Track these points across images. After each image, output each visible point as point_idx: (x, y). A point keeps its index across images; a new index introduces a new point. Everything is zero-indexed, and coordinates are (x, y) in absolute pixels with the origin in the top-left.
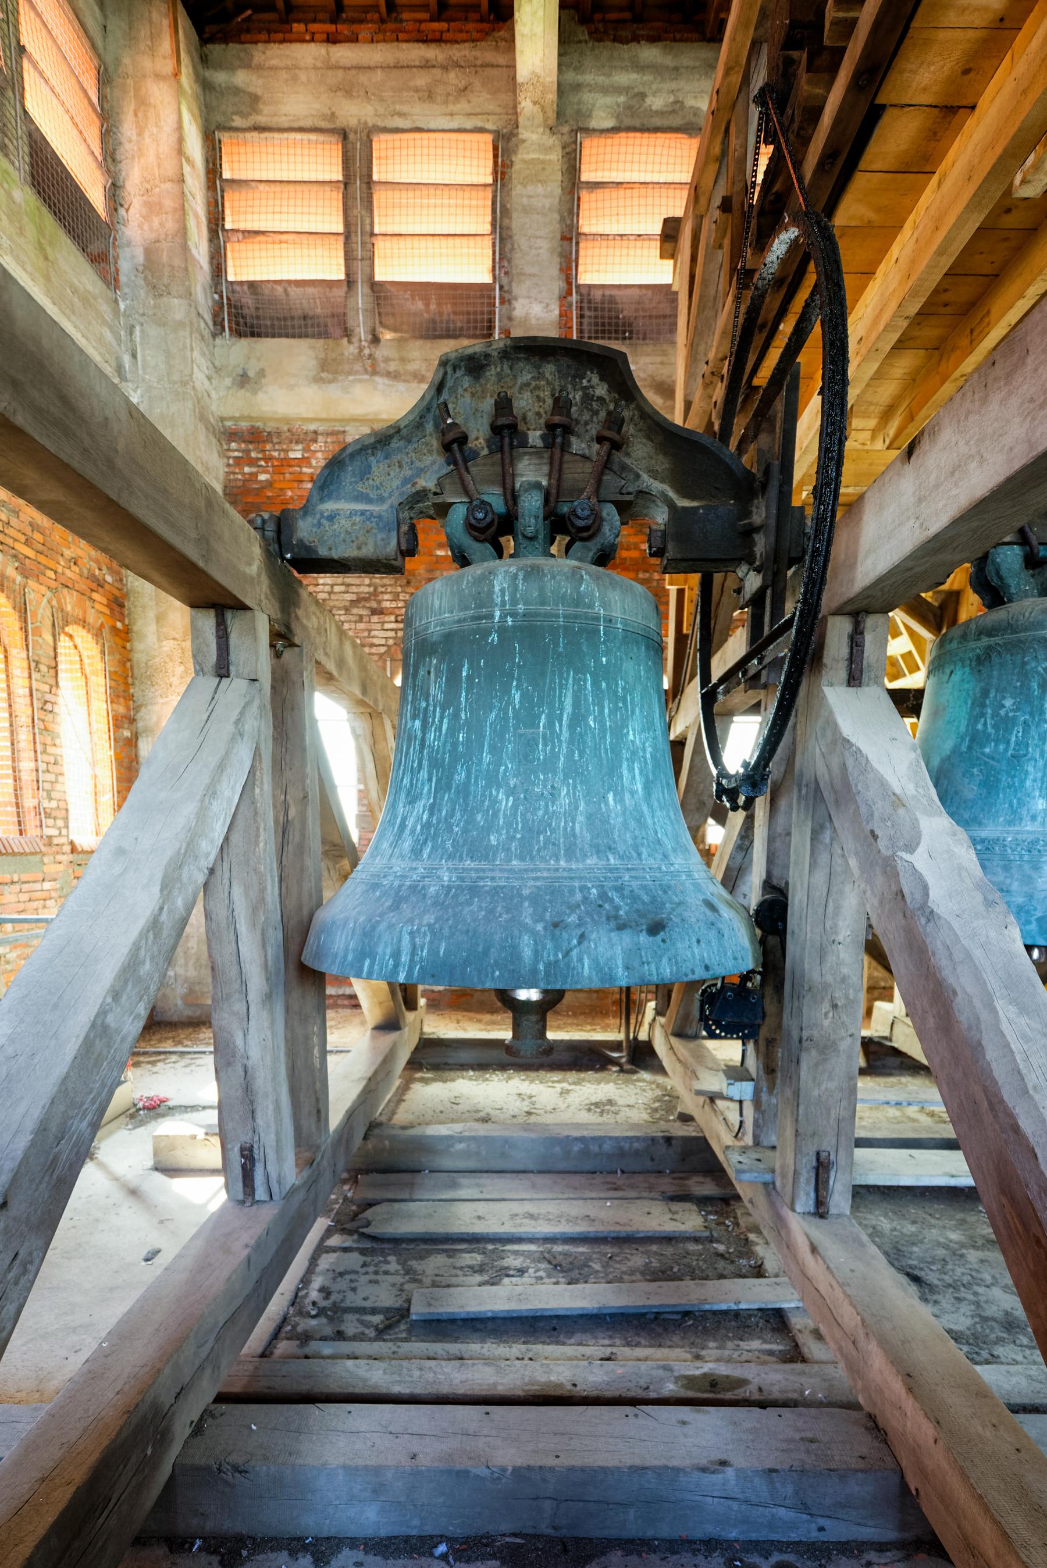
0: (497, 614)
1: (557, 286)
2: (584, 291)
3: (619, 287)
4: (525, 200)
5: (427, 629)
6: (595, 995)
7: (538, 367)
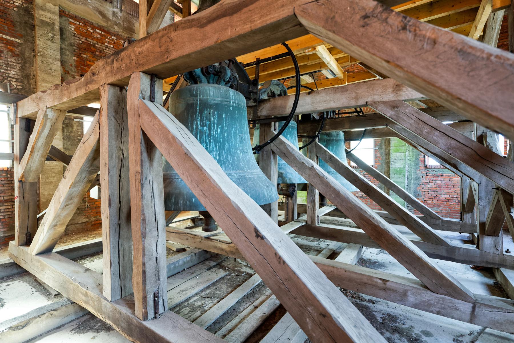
6: (84, 224)
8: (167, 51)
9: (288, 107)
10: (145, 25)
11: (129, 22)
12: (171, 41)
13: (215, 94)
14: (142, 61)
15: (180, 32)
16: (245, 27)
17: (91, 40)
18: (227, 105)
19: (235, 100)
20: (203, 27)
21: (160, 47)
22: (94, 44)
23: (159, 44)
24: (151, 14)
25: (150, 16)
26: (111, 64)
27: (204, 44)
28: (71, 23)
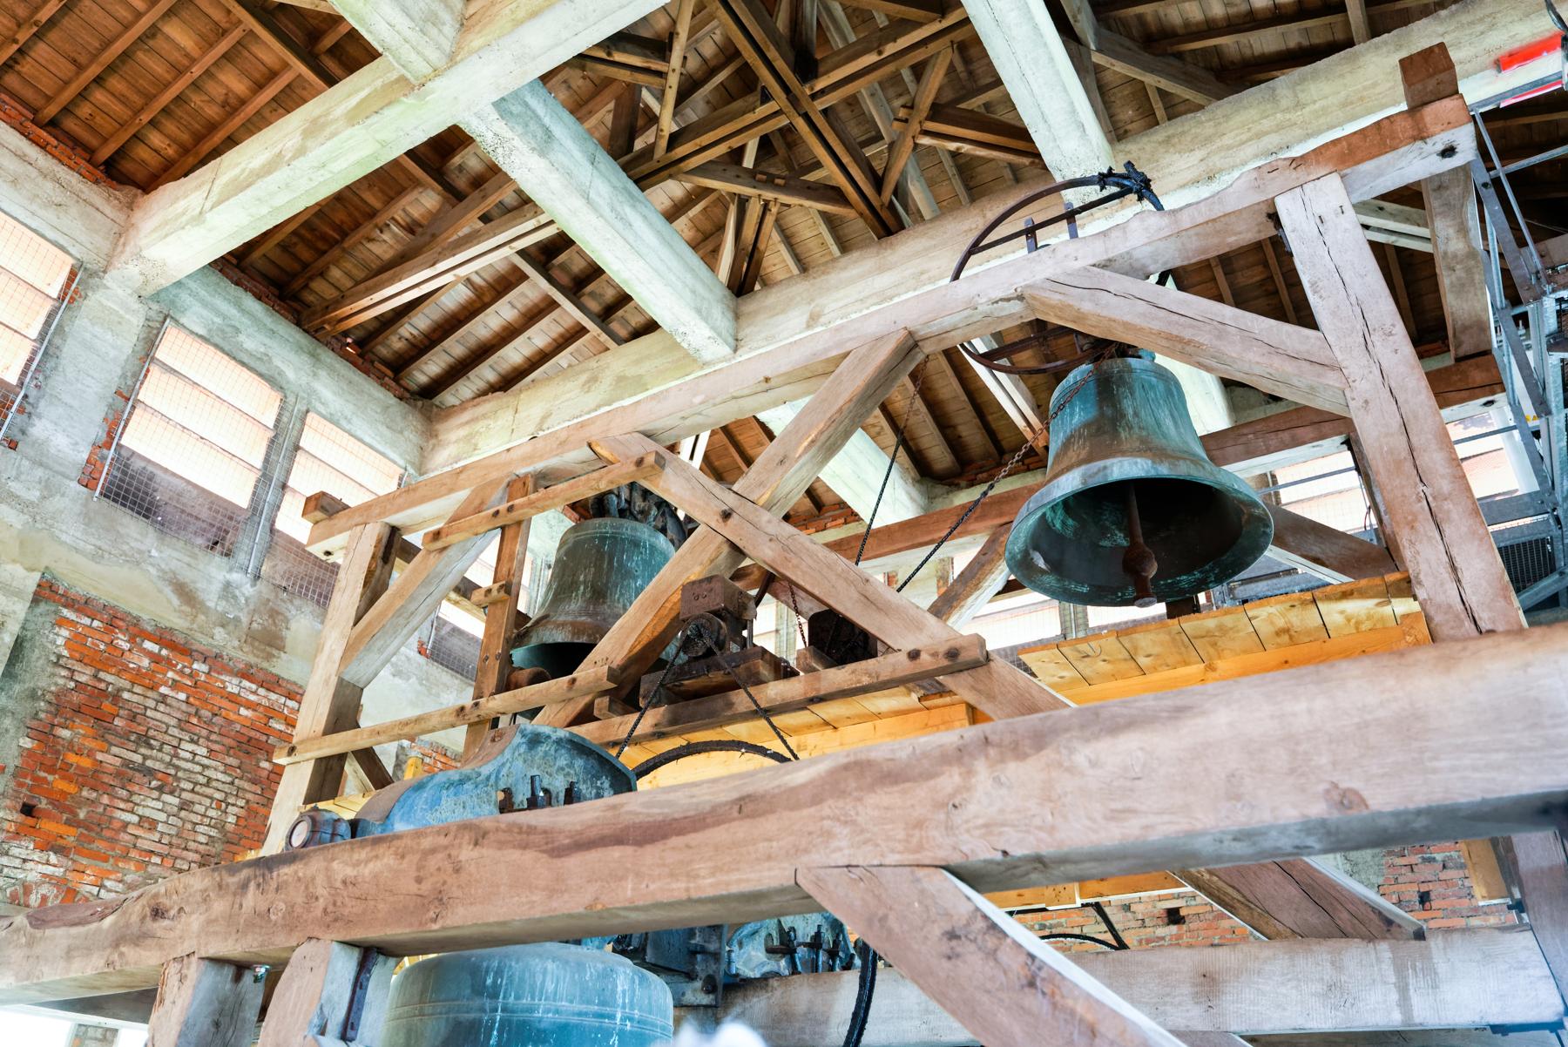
0: (619, 1016)
1: (97, 432)
2: (123, 452)
3: (166, 470)
4: (88, 336)
5: (531, 1010)
7: (573, 758)
8: (440, 899)
9: (834, 1021)
10: (338, 655)
11: (274, 614)
12: (457, 871)
13: (560, 988)
14: (351, 908)
15: (486, 852)
16: (674, 886)
17: (110, 678)
18: (600, 1029)
19: (632, 1008)
20: (559, 856)
21: (419, 880)
22: (120, 690)
23: (418, 869)
24: (370, 624)
25: (363, 631)
26: (235, 894)
27: (554, 904)
28: (62, 622)
